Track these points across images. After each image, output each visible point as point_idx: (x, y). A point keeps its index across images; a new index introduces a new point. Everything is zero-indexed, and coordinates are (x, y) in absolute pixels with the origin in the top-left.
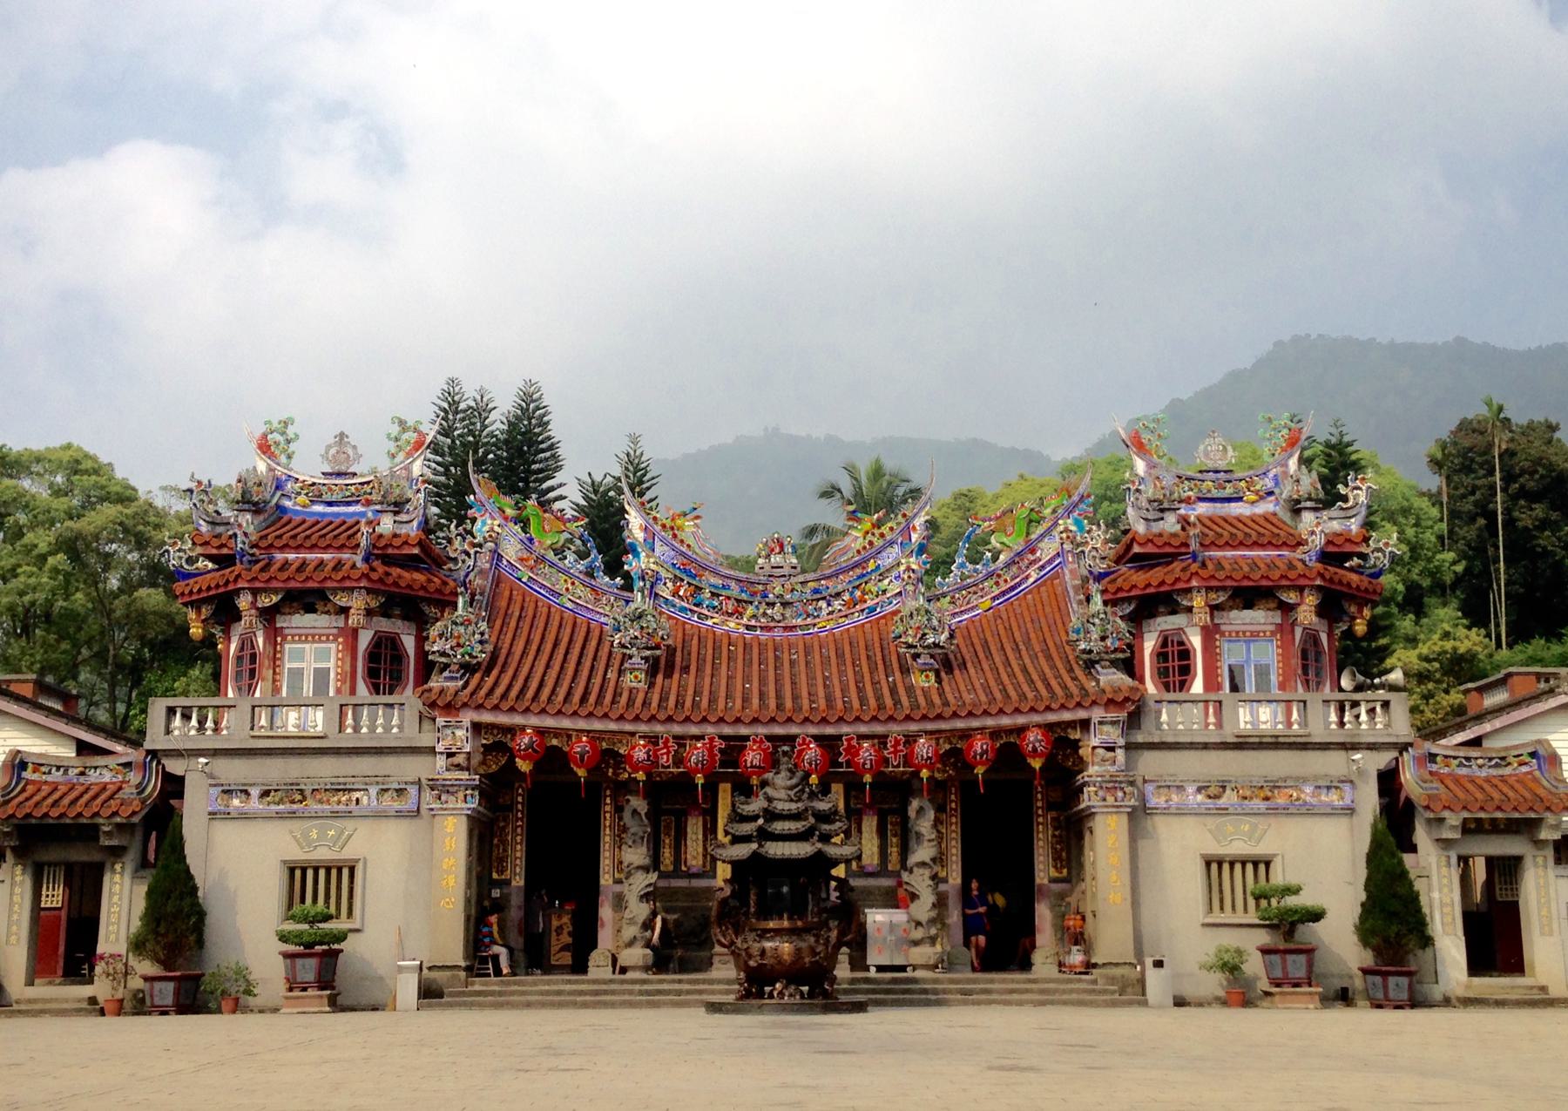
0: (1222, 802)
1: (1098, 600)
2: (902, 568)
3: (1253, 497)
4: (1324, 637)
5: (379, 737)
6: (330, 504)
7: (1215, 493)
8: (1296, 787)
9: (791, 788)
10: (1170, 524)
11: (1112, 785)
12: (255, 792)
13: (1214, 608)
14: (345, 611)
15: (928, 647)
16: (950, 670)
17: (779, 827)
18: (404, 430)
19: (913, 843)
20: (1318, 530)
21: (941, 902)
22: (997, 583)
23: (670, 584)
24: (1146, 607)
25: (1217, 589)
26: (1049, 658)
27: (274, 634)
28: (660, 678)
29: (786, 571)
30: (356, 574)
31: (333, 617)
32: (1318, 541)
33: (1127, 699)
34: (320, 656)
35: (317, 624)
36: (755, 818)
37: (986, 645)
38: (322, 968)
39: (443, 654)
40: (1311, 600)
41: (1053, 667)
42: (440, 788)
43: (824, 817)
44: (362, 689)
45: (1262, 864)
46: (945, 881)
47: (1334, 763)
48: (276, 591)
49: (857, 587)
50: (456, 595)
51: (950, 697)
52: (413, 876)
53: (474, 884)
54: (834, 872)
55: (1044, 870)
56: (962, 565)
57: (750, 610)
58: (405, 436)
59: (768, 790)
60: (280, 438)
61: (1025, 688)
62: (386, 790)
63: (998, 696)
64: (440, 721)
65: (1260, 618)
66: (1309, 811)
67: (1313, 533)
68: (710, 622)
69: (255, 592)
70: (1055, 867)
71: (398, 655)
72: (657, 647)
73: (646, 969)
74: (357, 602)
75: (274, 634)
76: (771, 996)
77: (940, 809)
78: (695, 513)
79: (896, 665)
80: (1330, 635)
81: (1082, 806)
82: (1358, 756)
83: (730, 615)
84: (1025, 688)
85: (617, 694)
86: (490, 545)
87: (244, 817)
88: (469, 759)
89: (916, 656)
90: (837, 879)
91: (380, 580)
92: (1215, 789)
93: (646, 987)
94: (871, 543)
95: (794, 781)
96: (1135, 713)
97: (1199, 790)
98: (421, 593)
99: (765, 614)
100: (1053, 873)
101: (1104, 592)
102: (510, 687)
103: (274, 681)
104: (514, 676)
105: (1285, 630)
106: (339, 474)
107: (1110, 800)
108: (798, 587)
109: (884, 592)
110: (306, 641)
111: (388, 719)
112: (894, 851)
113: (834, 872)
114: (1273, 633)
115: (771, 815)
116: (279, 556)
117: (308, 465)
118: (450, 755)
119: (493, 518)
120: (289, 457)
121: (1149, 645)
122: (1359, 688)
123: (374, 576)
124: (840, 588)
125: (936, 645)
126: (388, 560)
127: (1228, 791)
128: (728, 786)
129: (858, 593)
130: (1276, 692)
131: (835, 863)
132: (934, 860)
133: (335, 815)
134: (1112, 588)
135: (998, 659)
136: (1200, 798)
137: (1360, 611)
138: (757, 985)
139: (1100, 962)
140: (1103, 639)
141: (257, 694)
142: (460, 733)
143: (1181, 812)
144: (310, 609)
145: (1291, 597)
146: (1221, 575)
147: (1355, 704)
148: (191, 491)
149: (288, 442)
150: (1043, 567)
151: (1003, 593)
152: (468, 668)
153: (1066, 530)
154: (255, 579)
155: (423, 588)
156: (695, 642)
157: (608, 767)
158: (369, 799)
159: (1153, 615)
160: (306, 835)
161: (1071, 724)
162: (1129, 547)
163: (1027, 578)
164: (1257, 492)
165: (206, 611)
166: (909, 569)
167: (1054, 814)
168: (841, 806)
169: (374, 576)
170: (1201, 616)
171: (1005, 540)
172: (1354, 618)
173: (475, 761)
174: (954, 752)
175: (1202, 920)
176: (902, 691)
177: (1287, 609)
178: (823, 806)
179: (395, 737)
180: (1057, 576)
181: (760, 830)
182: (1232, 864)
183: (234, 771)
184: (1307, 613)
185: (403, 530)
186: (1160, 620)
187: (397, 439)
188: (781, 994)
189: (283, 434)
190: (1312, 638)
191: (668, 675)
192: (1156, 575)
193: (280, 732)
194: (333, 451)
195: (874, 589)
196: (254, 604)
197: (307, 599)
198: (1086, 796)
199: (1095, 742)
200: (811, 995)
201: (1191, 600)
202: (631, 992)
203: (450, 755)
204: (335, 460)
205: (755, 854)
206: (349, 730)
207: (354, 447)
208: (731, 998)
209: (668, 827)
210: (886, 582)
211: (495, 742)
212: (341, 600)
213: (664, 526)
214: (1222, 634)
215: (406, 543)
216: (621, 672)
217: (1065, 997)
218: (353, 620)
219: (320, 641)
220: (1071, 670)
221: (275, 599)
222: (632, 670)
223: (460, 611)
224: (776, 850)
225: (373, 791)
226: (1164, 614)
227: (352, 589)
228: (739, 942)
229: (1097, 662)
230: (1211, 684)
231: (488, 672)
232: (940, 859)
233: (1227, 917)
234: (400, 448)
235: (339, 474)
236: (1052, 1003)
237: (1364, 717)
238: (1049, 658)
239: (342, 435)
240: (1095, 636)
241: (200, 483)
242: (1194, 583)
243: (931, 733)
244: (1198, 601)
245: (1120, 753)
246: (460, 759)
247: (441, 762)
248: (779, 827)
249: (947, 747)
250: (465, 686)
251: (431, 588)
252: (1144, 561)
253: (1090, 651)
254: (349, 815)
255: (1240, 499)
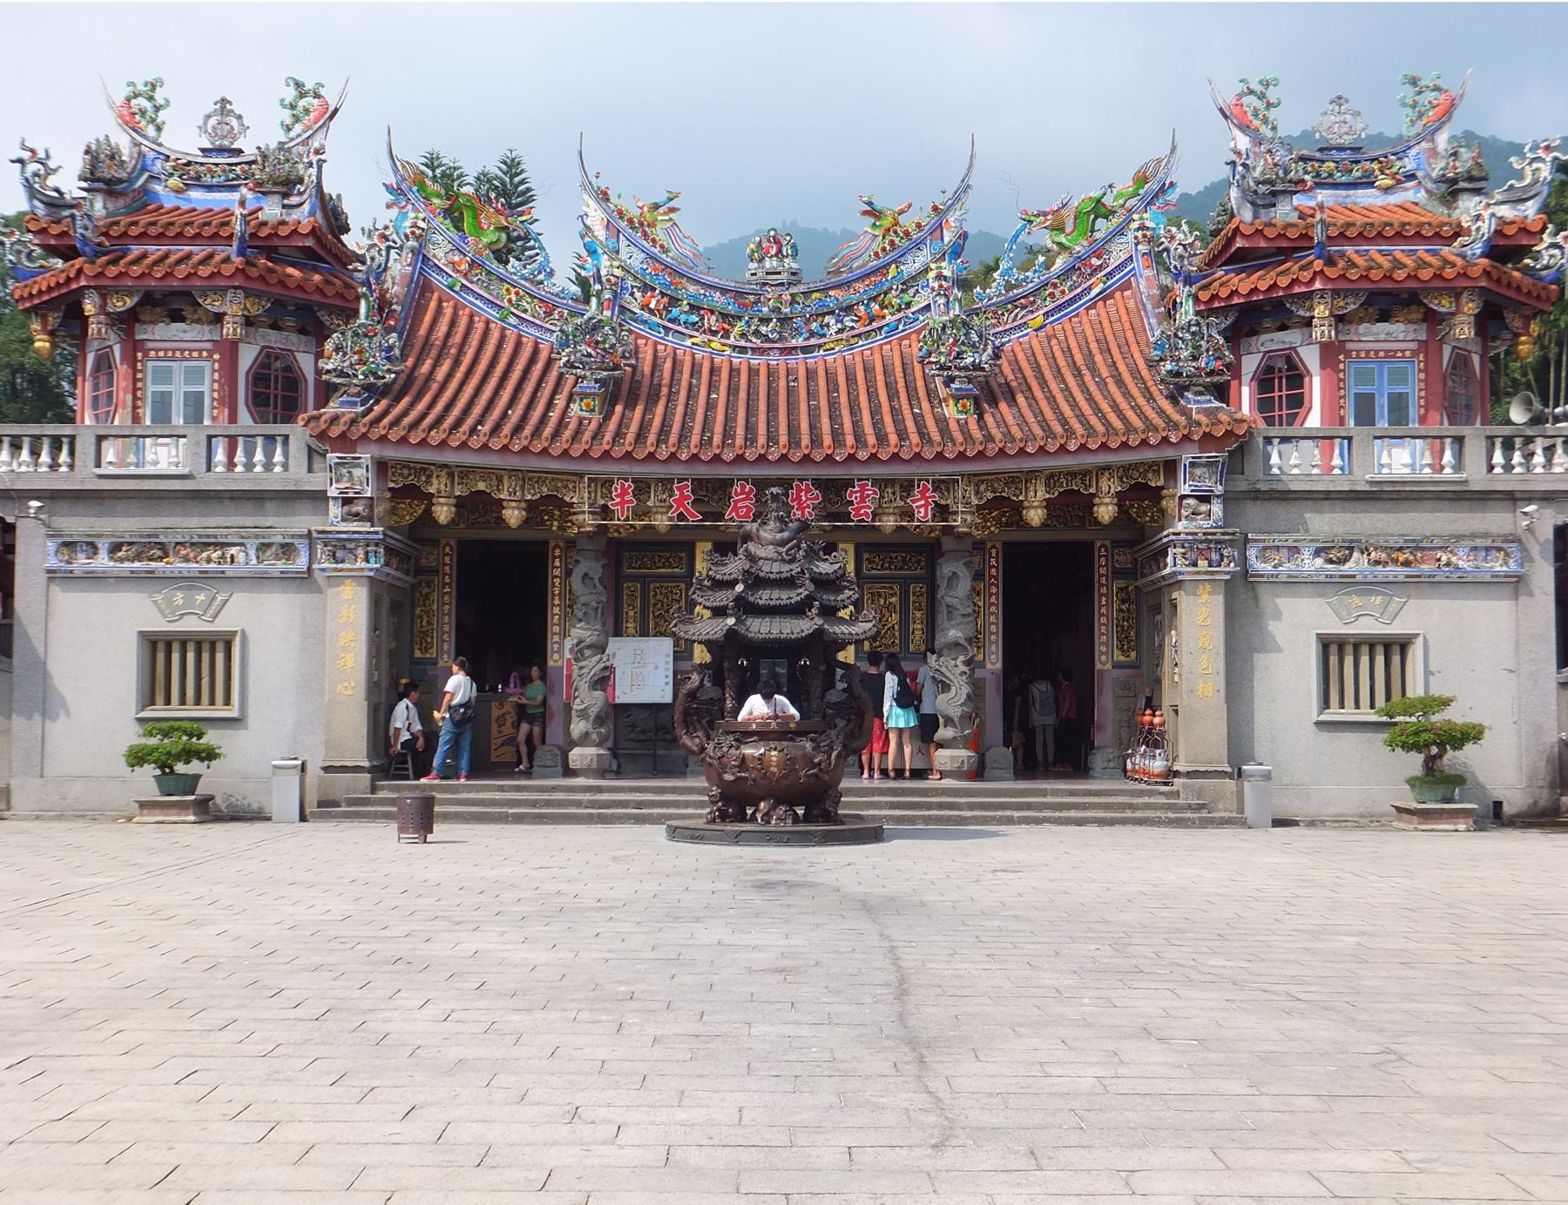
0: (1348, 567)
1: (1187, 312)
2: (932, 275)
3: (1389, 182)
4: (1476, 359)
5: (256, 479)
6: (210, 188)
7: (1339, 177)
8: (1443, 548)
9: (783, 543)
10: (1284, 212)
11: (1202, 546)
12: (103, 546)
13: (1340, 320)
14: (218, 318)
15: (966, 368)
16: (994, 402)
17: (765, 597)
18: (302, 95)
19: (942, 619)
20: (1486, 214)
21: (976, 695)
22: (1052, 295)
23: (638, 295)
24: (1247, 320)
25: (1347, 293)
26: (1120, 382)
27: (134, 348)
28: (619, 409)
29: (784, 277)
30: (228, 270)
31: (206, 328)
32: (1486, 228)
33: (1229, 434)
34: (194, 376)
35: (188, 336)
36: (732, 584)
37: (1037, 368)
38: (179, 774)
39: (342, 374)
40: (1471, 307)
41: (1127, 394)
42: (339, 547)
43: (822, 583)
44: (244, 417)
45: (1396, 647)
46: (982, 665)
47: (1496, 521)
48: (130, 293)
49: (874, 299)
50: (358, 299)
51: (994, 431)
52: (305, 653)
53: (385, 664)
54: (841, 656)
55: (1106, 656)
56: (1007, 272)
57: (739, 327)
58: (302, 103)
59: (751, 546)
60: (147, 105)
61: (1094, 420)
62: (269, 545)
63: (1057, 428)
64: (332, 457)
65: (1398, 333)
66: (1462, 584)
67: (1478, 217)
68: (688, 343)
69: (104, 293)
70: (1122, 649)
71: (292, 380)
72: (617, 367)
73: (602, 773)
74: (232, 307)
75: (134, 348)
76: (753, 819)
77: (978, 576)
78: (670, 205)
79: (922, 393)
80: (1482, 357)
81: (1168, 570)
82: (1531, 508)
83: (714, 333)
84: (1094, 420)
85: (562, 424)
86: (412, 243)
87: (94, 579)
88: (371, 507)
89: (949, 381)
90: (845, 666)
91: (261, 278)
92: (1337, 551)
93: (599, 797)
94: (892, 243)
95: (786, 534)
96: (1237, 450)
97: (1317, 553)
98: (318, 298)
99: (757, 333)
100: (1119, 657)
101: (1197, 300)
102: (424, 416)
103: (135, 407)
104: (431, 406)
105: (1428, 348)
106: (221, 150)
107: (1203, 564)
108: (800, 299)
109: (908, 305)
110: (173, 359)
111: (269, 454)
112: (917, 629)
113: (841, 656)
114: (1415, 353)
115: (757, 582)
116: (136, 250)
117: (184, 137)
118: (347, 501)
119: (416, 210)
120: (159, 129)
121: (1250, 364)
122: (1537, 420)
123: (254, 272)
124: (854, 298)
125: (976, 367)
126: (270, 252)
127: (1356, 554)
128: (708, 546)
129: (875, 307)
130: (1414, 425)
131: (842, 646)
132: (969, 640)
133: (205, 577)
134: (1204, 296)
135: (1053, 386)
136: (1319, 562)
137: (1527, 326)
138: (735, 807)
139: (1182, 769)
140: (1195, 358)
141: (116, 423)
142: (357, 472)
143: (1294, 584)
144: (177, 317)
145: (1443, 305)
146: (1353, 274)
147: (1529, 440)
148: (21, 161)
149: (157, 109)
150: (1110, 275)
151: (1060, 308)
152: (373, 391)
153: (1142, 227)
154: (101, 275)
155: (319, 290)
156: (668, 365)
157: (552, 518)
158: (245, 559)
159: (1254, 333)
160: (169, 602)
161: (1152, 466)
162: (1230, 241)
163: (1090, 288)
164: (1393, 176)
165: (53, 320)
166: (940, 277)
167: (1122, 583)
168: (851, 567)
169: (254, 272)
170: (1322, 331)
171: (1063, 240)
172: (1517, 335)
173: (379, 510)
174: (998, 502)
175: (1315, 718)
176: (930, 423)
177: (1433, 319)
178: (824, 568)
179: (277, 480)
180: (1126, 286)
181: (739, 599)
182: (1356, 647)
183: (76, 524)
184: (1464, 330)
185: (295, 215)
186: (1263, 337)
187: (293, 107)
188: (767, 818)
189: (151, 98)
190: (1461, 361)
191: (630, 405)
192: (1262, 280)
193: (149, 470)
194: (213, 121)
195: (895, 301)
196: (103, 306)
197: (173, 304)
198: (1169, 560)
199: (1185, 489)
200: (807, 819)
201: (1311, 308)
202: (579, 804)
203: (347, 501)
204: (214, 134)
205: (731, 633)
206: (220, 469)
207: (240, 117)
208: (700, 823)
209: (632, 596)
210: (911, 292)
211: (404, 487)
212: (213, 305)
213: (631, 221)
214: (1348, 354)
215: (295, 232)
216: (570, 399)
217: (1138, 814)
218: (229, 329)
219: (191, 359)
220: (1150, 398)
221: (130, 303)
222: (583, 396)
223: (362, 319)
224: (761, 628)
225: (252, 545)
226: (1268, 330)
227: (225, 289)
228: (710, 747)
229: (1187, 388)
230: (1333, 414)
231: (398, 399)
232: (976, 640)
233: (1349, 714)
234: (297, 119)
235: (221, 150)
236: (1124, 822)
237: (1539, 459)
238: (1120, 382)
239: (224, 101)
240: (1185, 354)
241: (33, 151)
242: (1318, 285)
243: (971, 476)
244: (1320, 311)
245: (1217, 508)
246: (359, 508)
247: (335, 510)
248: (765, 597)
249: (990, 495)
250: (364, 414)
251: (330, 291)
252: (1243, 259)
253: (1178, 374)
254: (221, 577)
255: (1371, 185)
